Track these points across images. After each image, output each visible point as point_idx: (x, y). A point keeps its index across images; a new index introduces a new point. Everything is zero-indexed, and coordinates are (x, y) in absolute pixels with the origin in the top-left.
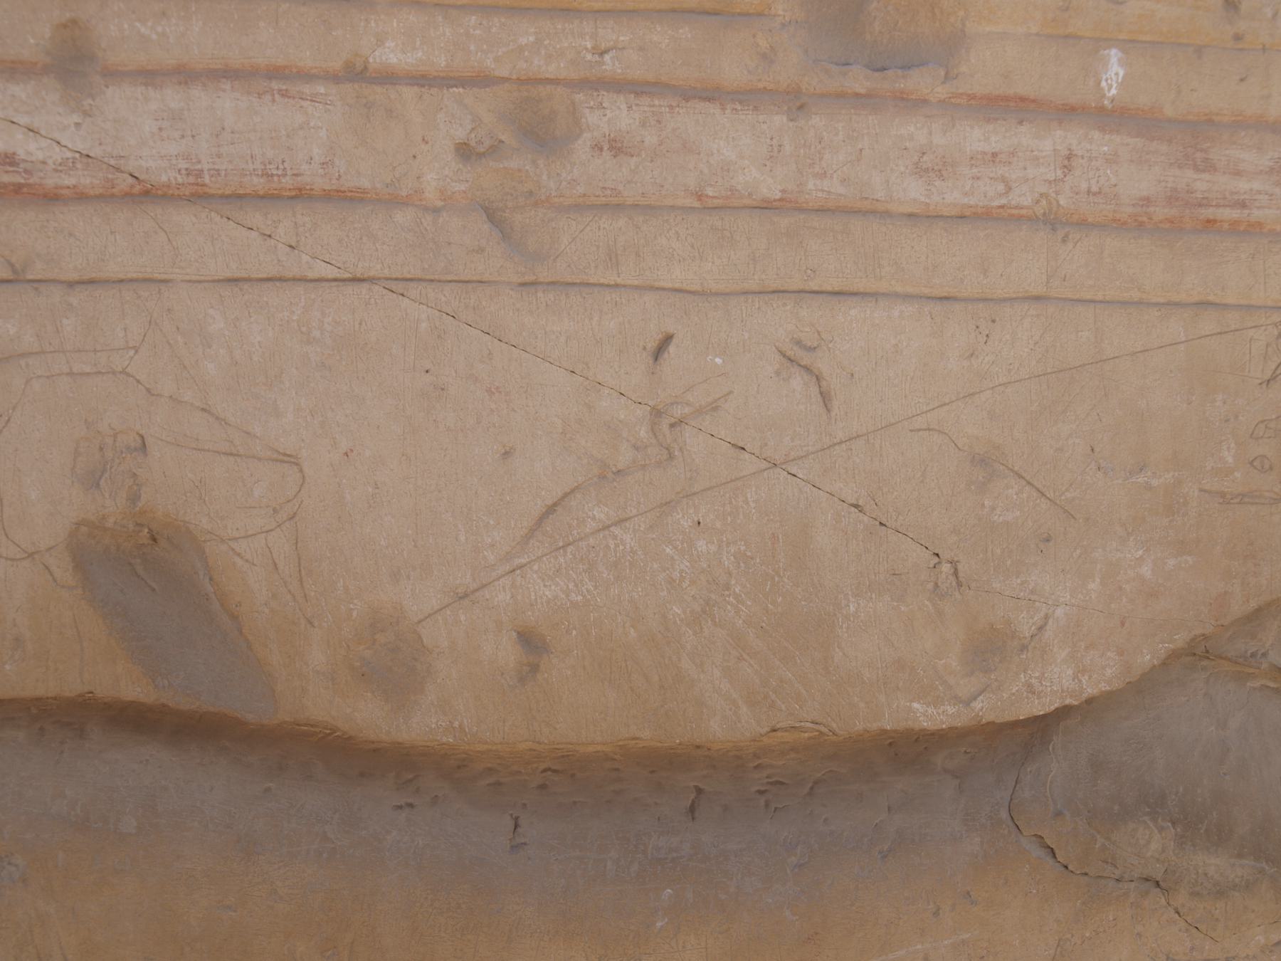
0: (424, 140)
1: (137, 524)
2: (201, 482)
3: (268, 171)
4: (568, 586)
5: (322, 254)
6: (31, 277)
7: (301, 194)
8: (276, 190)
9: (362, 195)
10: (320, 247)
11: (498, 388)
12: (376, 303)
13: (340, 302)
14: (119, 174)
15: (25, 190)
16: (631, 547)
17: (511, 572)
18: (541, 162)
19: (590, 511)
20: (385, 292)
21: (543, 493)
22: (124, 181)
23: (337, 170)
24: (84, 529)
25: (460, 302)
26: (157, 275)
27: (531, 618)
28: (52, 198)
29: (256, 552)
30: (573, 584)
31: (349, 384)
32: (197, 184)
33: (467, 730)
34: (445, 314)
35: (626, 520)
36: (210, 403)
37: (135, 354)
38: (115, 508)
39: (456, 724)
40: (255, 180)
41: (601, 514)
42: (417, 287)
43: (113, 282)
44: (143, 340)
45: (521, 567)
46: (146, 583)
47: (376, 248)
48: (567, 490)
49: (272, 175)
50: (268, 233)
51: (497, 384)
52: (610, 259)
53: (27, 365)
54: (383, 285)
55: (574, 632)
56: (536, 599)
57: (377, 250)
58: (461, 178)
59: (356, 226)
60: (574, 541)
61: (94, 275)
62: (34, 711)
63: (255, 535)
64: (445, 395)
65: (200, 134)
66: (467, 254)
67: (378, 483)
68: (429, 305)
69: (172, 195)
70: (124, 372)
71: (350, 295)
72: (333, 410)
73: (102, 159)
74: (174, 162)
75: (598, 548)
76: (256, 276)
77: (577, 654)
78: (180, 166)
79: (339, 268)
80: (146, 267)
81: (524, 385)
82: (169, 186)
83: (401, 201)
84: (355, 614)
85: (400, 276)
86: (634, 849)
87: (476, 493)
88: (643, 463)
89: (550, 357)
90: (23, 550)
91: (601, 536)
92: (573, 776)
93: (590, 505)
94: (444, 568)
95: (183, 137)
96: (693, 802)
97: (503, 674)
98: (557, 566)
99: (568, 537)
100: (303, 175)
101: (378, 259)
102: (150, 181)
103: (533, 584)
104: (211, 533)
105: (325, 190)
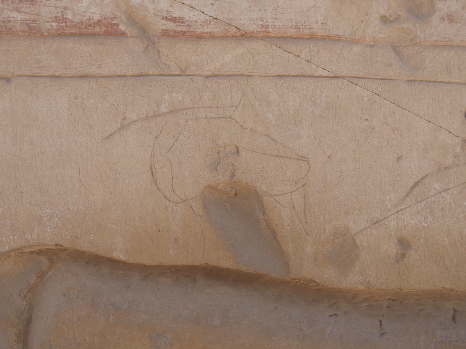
0: (366, 14)
1: (231, 188)
2: (263, 169)
3: (298, 26)
4: (421, 219)
5: (322, 65)
6: (188, 74)
7: (312, 37)
8: (301, 35)
9: (339, 39)
10: (320, 62)
11: (397, 128)
12: (345, 88)
13: (329, 88)
14: (230, 27)
15: (187, 34)
16: (449, 202)
17: (397, 212)
18: (417, 25)
19: (433, 185)
20: (349, 83)
21: (414, 176)
22: (233, 30)
23: (328, 27)
24: (208, 189)
25: (381, 88)
26: (247, 73)
27: (404, 233)
28: (199, 37)
29: (286, 201)
30: (423, 218)
31: (332, 125)
32: (266, 32)
33: (371, 283)
34: (374, 94)
35: (449, 189)
36: (269, 132)
37: (236, 109)
38: (224, 180)
39: (367, 280)
40: (292, 30)
41: (438, 186)
42: (363, 81)
43: (226, 76)
44: (240, 102)
45: (401, 210)
46: (231, 214)
47: (345, 63)
48: (424, 175)
49: (300, 28)
50: (297, 55)
51: (396, 126)
52: (447, 70)
53: (186, 114)
54: (348, 80)
55: (422, 240)
56: (407, 225)
57: (346, 64)
58: (382, 32)
59: (336, 52)
60: (426, 199)
61: (217, 73)
62: (173, 270)
63: (286, 193)
64: (374, 131)
65: (268, 9)
66: (385, 67)
67: (342, 171)
68: (368, 89)
69: (254, 37)
70: (230, 117)
71: (333, 84)
72: (324, 137)
73: (223, 20)
74: (255, 21)
75: (435, 202)
76: (292, 74)
77: (422, 249)
78: (258, 23)
79: (329, 72)
80: (242, 69)
81: (408, 127)
82: (253, 32)
83: (356, 42)
84: (327, 230)
85: (355, 76)
86: (432, 336)
87: (385, 176)
88: (457, 164)
89: (420, 114)
90: (181, 199)
91: (437, 196)
92: (401, 302)
93: (433, 182)
94: (368, 210)
95: (260, 10)
96: (453, 315)
97: (389, 258)
98: (417, 210)
99: (423, 197)
100: (313, 28)
101: (346, 68)
102: (244, 30)
103: (406, 218)
104: (266, 192)
105: (323, 36)
